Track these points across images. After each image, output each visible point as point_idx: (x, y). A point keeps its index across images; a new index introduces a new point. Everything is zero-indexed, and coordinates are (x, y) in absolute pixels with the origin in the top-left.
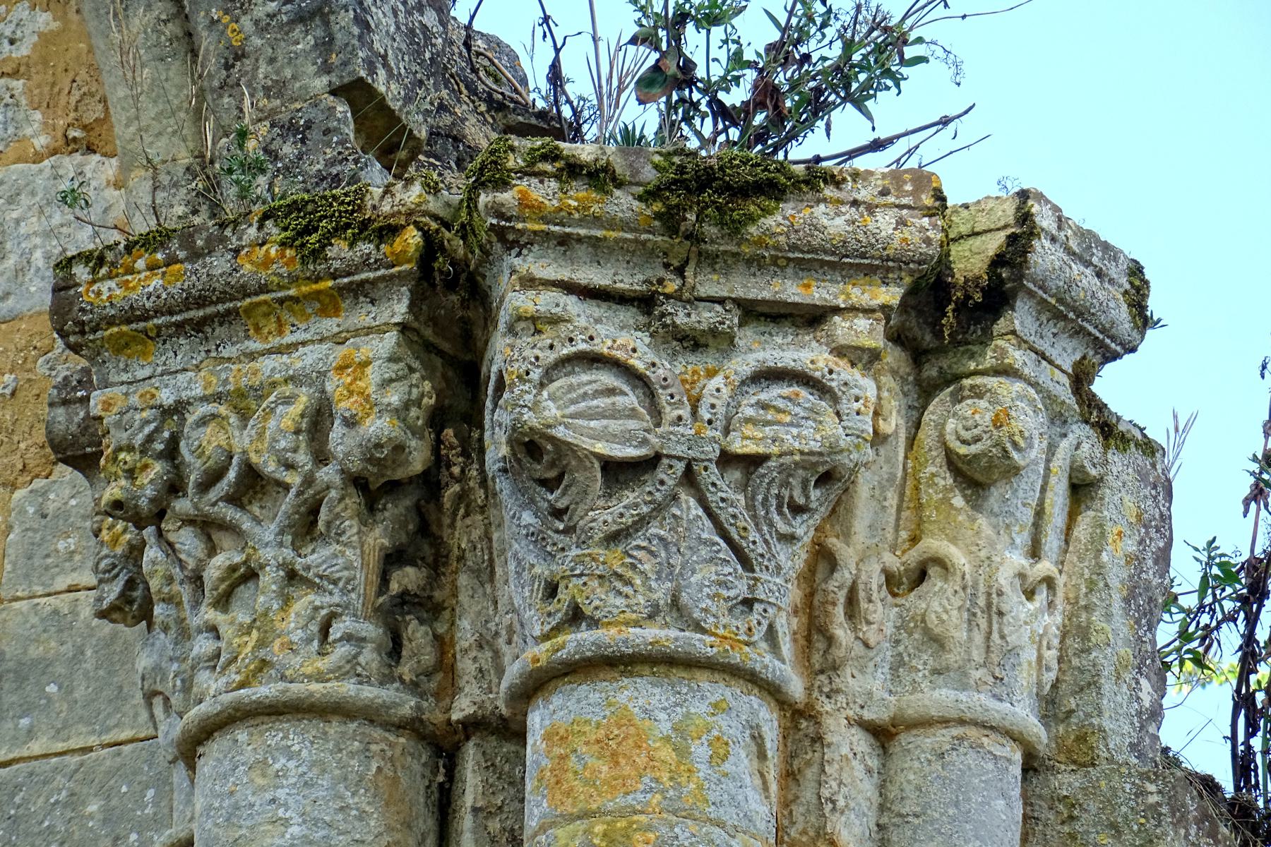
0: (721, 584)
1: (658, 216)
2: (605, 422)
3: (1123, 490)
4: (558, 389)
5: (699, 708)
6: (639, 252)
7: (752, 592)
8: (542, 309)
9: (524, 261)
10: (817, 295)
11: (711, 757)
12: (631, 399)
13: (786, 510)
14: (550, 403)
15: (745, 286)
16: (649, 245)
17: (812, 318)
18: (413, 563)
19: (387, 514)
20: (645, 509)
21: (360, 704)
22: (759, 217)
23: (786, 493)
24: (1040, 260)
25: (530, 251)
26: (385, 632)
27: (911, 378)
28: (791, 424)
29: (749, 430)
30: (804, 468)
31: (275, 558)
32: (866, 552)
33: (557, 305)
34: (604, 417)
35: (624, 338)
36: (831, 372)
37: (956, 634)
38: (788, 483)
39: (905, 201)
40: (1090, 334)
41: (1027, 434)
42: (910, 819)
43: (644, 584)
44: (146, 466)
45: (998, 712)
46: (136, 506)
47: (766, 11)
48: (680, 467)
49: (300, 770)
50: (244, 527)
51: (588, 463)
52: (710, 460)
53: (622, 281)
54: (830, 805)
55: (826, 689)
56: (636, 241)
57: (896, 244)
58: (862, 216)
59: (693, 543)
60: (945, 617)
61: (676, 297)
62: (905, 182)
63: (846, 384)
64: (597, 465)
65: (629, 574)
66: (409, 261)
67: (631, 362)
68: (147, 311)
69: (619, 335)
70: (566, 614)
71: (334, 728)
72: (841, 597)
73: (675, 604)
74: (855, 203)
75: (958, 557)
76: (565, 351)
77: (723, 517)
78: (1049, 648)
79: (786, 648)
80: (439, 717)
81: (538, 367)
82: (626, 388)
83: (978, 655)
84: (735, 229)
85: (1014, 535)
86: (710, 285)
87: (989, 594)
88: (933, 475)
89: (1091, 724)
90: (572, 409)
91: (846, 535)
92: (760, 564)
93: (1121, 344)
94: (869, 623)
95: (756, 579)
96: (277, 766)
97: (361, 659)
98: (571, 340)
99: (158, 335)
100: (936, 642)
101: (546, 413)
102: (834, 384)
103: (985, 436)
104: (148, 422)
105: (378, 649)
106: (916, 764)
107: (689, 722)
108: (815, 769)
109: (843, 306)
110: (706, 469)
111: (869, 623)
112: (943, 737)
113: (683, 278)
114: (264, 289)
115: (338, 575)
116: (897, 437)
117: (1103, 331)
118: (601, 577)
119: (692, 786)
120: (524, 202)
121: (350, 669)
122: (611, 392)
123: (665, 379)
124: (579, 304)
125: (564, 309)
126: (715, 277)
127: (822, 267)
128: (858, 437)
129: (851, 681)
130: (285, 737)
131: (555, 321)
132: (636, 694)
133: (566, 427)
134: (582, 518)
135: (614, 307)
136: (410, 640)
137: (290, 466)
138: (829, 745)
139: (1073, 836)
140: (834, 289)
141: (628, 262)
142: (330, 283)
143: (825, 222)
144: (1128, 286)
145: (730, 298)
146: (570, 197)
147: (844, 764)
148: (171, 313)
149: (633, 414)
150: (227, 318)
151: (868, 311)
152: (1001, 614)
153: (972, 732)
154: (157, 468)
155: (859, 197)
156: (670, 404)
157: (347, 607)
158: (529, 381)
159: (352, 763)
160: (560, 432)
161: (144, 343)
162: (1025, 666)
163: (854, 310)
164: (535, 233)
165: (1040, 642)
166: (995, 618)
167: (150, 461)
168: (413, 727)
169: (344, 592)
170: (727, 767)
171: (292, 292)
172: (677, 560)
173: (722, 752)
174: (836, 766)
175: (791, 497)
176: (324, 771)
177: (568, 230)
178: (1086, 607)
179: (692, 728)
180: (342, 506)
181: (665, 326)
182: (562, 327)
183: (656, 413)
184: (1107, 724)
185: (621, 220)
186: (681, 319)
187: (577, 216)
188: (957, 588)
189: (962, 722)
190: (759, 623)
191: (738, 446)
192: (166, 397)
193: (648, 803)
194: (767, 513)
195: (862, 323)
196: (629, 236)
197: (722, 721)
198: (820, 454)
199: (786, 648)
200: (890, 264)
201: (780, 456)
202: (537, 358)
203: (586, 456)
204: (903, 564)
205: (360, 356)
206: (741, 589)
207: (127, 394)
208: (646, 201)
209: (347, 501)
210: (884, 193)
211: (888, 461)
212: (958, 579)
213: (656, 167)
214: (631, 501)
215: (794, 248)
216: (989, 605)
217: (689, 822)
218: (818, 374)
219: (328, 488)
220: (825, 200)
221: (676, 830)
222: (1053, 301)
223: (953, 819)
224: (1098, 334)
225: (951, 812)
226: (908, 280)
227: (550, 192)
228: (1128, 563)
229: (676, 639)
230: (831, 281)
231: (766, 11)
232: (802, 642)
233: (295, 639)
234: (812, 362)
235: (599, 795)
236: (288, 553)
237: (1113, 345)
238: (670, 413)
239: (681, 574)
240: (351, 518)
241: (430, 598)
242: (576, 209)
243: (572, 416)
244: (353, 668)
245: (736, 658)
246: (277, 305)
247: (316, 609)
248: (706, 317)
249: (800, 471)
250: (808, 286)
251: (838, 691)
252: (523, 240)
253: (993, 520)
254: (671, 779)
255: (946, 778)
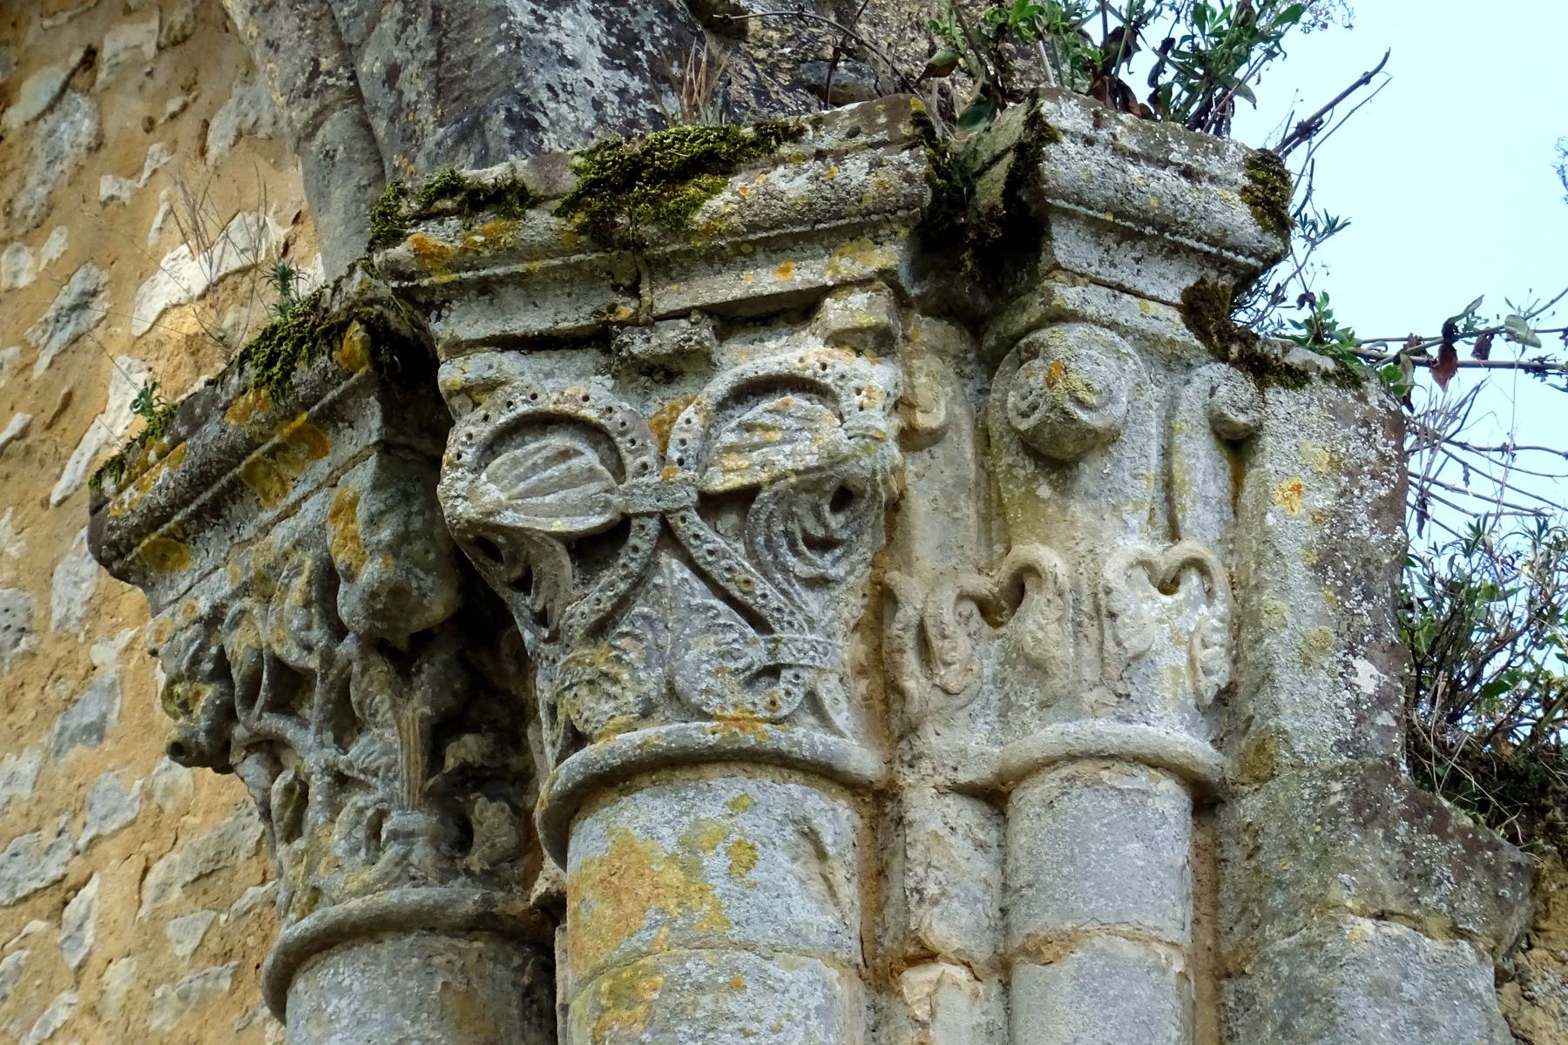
0: (722, 655)
1: (582, 229)
2: (562, 493)
3: (1300, 435)
4: (499, 467)
5: (711, 812)
6: (574, 279)
7: (774, 658)
8: (472, 376)
9: (446, 324)
10: (798, 279)
11: (731, 867)
12: (590, 458)
13: (803, 547)
14: (491, 486)
15: (712, 289)
16: (586, 268)
17: (798, 309)
18: (474, 729)
19: (423, 677)
20: (622, 587)
21: (406, 910)
22: (703, 199)
23: (795, 527)
24: (1062, 169)
25: (450, 310)
26: (442, 821)
27: (971, 356)
28: (783, 442)
29: (732, 461)
30: (807, 491)
31: (317, 763)
32: (936, 579)
33: (490, 367)
34: (562, 488)
35: (576, 388)
36: (824, 367)
37: (1058, 653)
38: (793, 515)
39: (877, 137)
40: (1193, 250)
41: (1097, 387)
42: (63, 819)
43: (632, 676)
44: (198, 694)
45: (1117, 735)
46: (198, 744)
47: (1387, 55)
48: (653, 525)
49: (352, 1007)
50: (289, 735)
51: (548, 549)
52: (686, 508)
53: (565, 320)
54: (916, 896)
55: (907, 758)
56: (566, 266)
57: (872, 190)
58: (828, 168)
59: (683, 614)
60: (1040, 635)
61: (633, 322)
62: (878, 115)
63: (843, 377)
64: (559, 547)
65: (614, 669)
66: (362, 364)
67: (583, 413)
68: (164, 508)
69: (579, 386)
70: (565, 738)
71: (387, 948)
72: (909, 639)
73: (673, 693)
74: (820, 155)
75: (1051, 559)
76: (503, 420)
77: (715, 572)
78: (1205, 646)
79: (842, 717)
80: (519, 906)
81: (471, 445)
82: (580, 446)
83: (1089, 674)
84: (676, 222)
85: (1125, 516)
86: (670, 297)
87: (1095, 595)
88: (1011, 466)
89: (1269, 727)
90: (522, 486)
91: (907, 564)
92: (779, 621)
93: (1251, 255)
94: (947, 664)
95: (776, 641)
96: (330, 1010)
97: (414, 859)
98: (510, 404)
99: (187, 535)
100: (1038, 668)
101: (486, 499)
102: (828, 381)
103: (1041, 401)
104: (192, 641)
105: (435, 841)
106: (1027, 823)
107: (698, 832)
108: (900, 858)
109: (831, 283)
110: (683, 519)
111: (947, 664)
112: (1049, 783)
113: (639, 297)
114: (252, 445)
115: (375, 765)
116: (958, 429)
117: (1213, 242)
118: (591, 682)
119: (707, 907)
120: (421, 253)
121: (402, 872)
122: (565, 455)
123: (623, 424)
124: (523, 359)
125: (499, 370)
126: (675, 287)
127: (796, 243)
128: (864, 437)
129: (933, 740)
130: (336, 973)
131: (491, 386)
132: (636, 813)
133: (515, 510)
134: (561, 617)
135: (569, 353)
136: (481, 824)
137: (309, 648)
138: (911, 824)
139: (1257, 871)
140: (818, 266)
141: (569, 295)
142: (304, 416)
143: (782, 185)
144: (1247, 182)
145: (695, 308)
146: (475, 233)
147: (932, 842)
148: (186, 504)
149: (592, 475)
150: (235, 490)
151: (863, 283)
152: (1112, 615)
153: (1086, 768)
154: (209, 691)
155: (823, 146)
156: (630, 452)
157: (391, 800)
158: (461, 466)
159: (410, 984)
160: (508, 518)
161: (177, 549)
162: (1167, 674)
163: (845, 286)
164: (445, 285)
165: (1191, 640)
166: (1107, 622)
167: (201, 686)
168: (482, 924)
169: (388, 781)
170: (755, 875)
171: (276, 440)
172: (666, 639)
173: (745, 859)
174: (920, 847)
175: (804, 531)
176: (377, 1002)
177: (482, 273)
178: (1256, 587)
179: (703, 838)
180: (367, 678)
181: (623, 360)
182: (499, 392)
183: (619, 471)
184: (1287, 723)
185: (541, 245)
186: (639, 348)
187: (487, 253)
188: (1050, 596)
189: (1072, 758)
190: (788, 693)
191: (720, 482)
192: (203, 606)
193: (654, 942)
194: (776, 557)
195: (859, 299)
196: (557, 262)
197: (745, 822)
198: (819, 469)
199: (842, 717)
200: (874, 217)
201: (772, 482)
202: (470, 436)
203: (543, 539)
204: (997, 584)
205: (349, 495)
206: (757, 654)
207: (173, 615)
208: (565, 215)
209: (372, 671)
210: (853, 133)
211: (950, 461)
212: (1050, 585)
213: (578, 171)
214: (611, 580)
215: (753, 227)
216: (1097, 609)
217: (704, 952)
218: (808, 373)
219: (350, 662)
220: (783, 161)
221: (688, 965)
222: (1110, 218)
223: (1068, 878)
224: (1206, 248)
225: (1065, 871)
226: (903, 232)
227: (450, 232)
228: (1316, 522)
229: (668, 734)
230: (813, 257)
231: (1387, 55)
232: (880, 707)
233: (339, 852)
234: (801, 360)
235: (606, 946)
236: (330, 752)
237: (1241, 258)
238: (632, 463)
239: (673, 655)
240: (381, 691)
241: (506, 767)
242: (483, 245)
243: (522, 496)
244: (405, 870)
245: (750, 740)
246: (270, 460)
247: (360, 811)
248: (669, 337)
249: (804, 496)
250: (786, 270)
251: (920, 757)
252: (438, 299)
253: (1091, 503)
254: (679, 905)
255: (1058, 830)
